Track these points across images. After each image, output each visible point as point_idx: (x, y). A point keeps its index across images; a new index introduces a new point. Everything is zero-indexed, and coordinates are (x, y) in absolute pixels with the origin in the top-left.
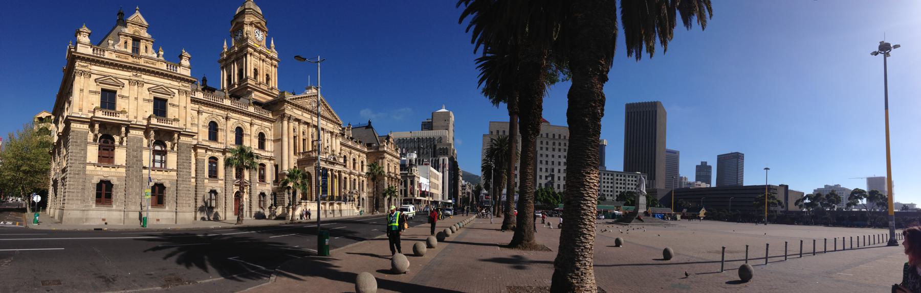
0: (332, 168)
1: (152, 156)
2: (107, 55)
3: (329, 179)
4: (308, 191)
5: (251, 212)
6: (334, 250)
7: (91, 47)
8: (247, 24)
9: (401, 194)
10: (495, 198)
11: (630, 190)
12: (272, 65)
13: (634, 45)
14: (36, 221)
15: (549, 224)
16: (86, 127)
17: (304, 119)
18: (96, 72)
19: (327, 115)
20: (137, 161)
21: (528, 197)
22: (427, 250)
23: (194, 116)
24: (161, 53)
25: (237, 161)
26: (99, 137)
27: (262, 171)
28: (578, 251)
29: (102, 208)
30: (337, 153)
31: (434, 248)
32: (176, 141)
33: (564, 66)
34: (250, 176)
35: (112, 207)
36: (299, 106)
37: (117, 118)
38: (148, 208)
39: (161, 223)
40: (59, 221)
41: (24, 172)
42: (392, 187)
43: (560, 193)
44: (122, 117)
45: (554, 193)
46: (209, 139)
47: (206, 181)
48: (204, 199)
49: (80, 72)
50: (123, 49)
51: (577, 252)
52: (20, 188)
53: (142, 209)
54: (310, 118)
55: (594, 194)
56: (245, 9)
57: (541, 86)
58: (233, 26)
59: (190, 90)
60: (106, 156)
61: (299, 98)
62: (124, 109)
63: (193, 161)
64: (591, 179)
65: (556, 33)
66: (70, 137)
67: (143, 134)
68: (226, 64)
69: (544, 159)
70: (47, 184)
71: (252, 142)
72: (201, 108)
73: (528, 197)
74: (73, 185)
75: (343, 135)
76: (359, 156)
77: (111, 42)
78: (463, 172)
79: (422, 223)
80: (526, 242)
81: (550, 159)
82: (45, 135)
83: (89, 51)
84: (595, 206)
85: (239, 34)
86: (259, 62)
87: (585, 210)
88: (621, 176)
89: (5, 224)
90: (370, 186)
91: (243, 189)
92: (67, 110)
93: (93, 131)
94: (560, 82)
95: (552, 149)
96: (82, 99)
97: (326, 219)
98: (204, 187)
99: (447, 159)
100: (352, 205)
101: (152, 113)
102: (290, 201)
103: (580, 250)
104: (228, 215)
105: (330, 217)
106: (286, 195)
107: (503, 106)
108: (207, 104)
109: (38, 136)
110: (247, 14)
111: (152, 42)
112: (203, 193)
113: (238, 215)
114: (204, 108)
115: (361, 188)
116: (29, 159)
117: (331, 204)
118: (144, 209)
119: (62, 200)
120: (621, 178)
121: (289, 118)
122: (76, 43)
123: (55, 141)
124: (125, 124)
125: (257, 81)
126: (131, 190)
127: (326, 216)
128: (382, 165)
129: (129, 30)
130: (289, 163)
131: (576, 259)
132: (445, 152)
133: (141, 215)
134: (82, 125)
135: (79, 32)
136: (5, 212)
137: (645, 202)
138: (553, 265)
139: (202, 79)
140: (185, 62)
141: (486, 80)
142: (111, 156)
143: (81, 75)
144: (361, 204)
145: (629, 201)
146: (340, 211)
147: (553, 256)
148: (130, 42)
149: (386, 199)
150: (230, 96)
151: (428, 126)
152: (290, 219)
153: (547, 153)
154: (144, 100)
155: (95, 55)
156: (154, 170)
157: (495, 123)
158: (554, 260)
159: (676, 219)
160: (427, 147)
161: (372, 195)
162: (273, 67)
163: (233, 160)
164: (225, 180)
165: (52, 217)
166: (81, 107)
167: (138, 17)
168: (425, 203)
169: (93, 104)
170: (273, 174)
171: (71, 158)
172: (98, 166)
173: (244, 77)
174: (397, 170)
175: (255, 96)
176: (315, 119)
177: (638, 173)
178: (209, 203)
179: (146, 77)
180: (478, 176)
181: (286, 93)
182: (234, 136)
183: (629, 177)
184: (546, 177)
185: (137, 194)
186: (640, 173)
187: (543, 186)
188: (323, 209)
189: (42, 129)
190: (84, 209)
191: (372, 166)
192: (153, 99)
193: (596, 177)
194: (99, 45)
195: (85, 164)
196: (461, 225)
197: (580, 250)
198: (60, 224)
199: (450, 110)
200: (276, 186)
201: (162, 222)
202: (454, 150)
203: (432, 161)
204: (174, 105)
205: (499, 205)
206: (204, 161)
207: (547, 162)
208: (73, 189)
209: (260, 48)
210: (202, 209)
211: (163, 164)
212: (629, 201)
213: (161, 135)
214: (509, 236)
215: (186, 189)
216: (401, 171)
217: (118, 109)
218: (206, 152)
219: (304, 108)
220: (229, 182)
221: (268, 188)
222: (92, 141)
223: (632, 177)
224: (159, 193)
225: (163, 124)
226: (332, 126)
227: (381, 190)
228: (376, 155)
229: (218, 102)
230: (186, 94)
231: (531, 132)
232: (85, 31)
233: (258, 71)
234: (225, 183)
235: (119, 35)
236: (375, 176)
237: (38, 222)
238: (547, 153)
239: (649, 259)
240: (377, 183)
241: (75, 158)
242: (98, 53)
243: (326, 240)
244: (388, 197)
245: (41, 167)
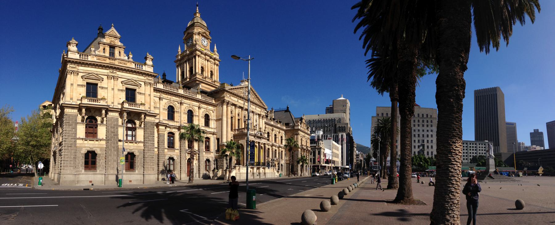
0: (259, 141)
1: (125, 132)
2: (90, 58)
3: (256, 150)
4: (241, 158)
5: (199, 174)
6: (260, 204)
7: (78, 54)
8: (196, 34)
9: (311, 162)
10: (381, 164)
11: (481, 154)
12: (215, 64)
13: (483, 44)
14: (40, 184)
15: (422, 183)
16: (76, 111)
17: (239, 104)
18: (82, 71)
19: (256, 101)
20: (114, 135)
21: (407, 163)
22: (331, 206)
23: (156, 101)
24: (131, 56)
25: (188, 135)
26: (85, 118)
27: (208, 143)
28: (447, 206)
29: (89, 172)
30: (263, 130)
31: (336, 204)
32: (143, 120)
33: (430, 62)
34: (199, 146)
35: (97, 171)
36: (235, 95)
37: (98, 104)
38: (122, 172)
39: (132, 184)
40: (58, 183)
41: (33, 146)
42: (304, 157)
43: (429, 158)
44: (102, 103)
45: (425, 158)
46: (168, 119)
47: (166, 150)
48: (164, 165)
49: (70, 71)
50: (102, 54)
51: (447, 207)
52: (30, 158)
53: (118, 173)
54: (237, 101)
55: (459, 159)
56: (194, 23)
57: (414, 78)
58: (186, 35)
59: (153, 82)
60: (91, 133)
61: (235, 88)
62: (104, 96)
63: (156, 135)
64: (457, 147)
65: (424, 37)
66: (64, 119)
67: (118, 115)
68: (180, 63)
69: (417, 133)
70: (49, 155)
71: (200, 121)
72: (162, 95)
73: (407, 163)
74: (67, 155)
75: (267, 116)
76: (279, 133)
77: (93, 49)
78: (357, 144)
79: (327, 184)
80: (407, 198)
81: (421, 133)
82: (47, 118)
83: (77, 56)
84: (460, 169)
85: (190, 42)
86: (204, 61)
87: (452, 172)
88: (473, 144)
89: (18, 186)
90: (287, 155)
91: (193, 156)
92: (62, 100)
93: (81, 114)
94: (427, 75)
95: (422, 126)
96: (72, 91)
97: (254, 180)
98: (165, 155)
99: (345, 135)
100: (274, 169)
101: (125, 100)
102: (227, 166)
103: (449, 205)
104: (182, 176)
105: (257, 178)
106: (225, 161)
107: (387, 94)
108: (166, 92)
109: (43, 119)
110: (196, 26)
111: (124, 48)
112: (163, 159)
113: (190, 176)
114: (164, 96)
115: (280, 156)
116: (36, 136)
117: (258, 169)
118: (120, 172)
119: (59, 167)
120: (473, 146)
121: (228, 103)
122: (67, 51)
123: (54, 122)
124: (105, 108)
125: (203, 76)
126: (110, 158)
127: (254, 178)
128: (297, 139)
129: (106, 40)
130: (227, 137)
131: (446, 213)
132: (343, 129)
133: (117, 177)
134: (73, 110)
135: (70, 44)
136: (19, 176)
137: (494, 163)
138: (429, 217)
139: (162, 74)
140: (149, 62)
141: (374, 75)
142: (95, 132)
143: (72, 74)
144: (280, 169)
145: (480, 163)
146: (265, 173)
147: (428, 209)
148: (108, 49)
149: (299, 166)
150: (183, 87)
151: (330, 110)
152: (227, 179)
153: (419, 128)
154: (119, 90)
155: (81, 59)
156: (127, 142)
157: (381, 108)
158: (430, 213)
159: (519, 176)
160: (330, 126)
161: (288, 162)
162: (216, 66)
163: (185, 135)
164: (180, 150)
165: (53, 180)
166: (72, 96)
167: (113, 31)
168: (329, 169)
169: (80, 94)
170: (215, 145)
171: (65, 134)
172: (85, 140)
173: (194, 73)
174: (308, 143)
175: (202, 86)
176: (246, 104)
177: (486, 141)
178: (168, 167)
179: (119, 74)
180: (368, 147)
181: (225, 85)
182: (186, 116)
183: (480, 144)
184: (419, 147)
185: (114, 161)
186: (488, 141)
187: (417, 154)
188: (252, 172)
189: (45, 114)
190: (75, 173)
191: (289, 140)
192: (125, 89)
193: (460, 145)
194: (84, 51)
195: (76, 139)
196: (356, 185)
197: (449, 205)
198: (58, 185)
199: (347, 98)
200: (218, 155)
201: (134, 183)
202: (350, 128)
203: (333, 136)
204: (140, 93)
205: (384, 169)
206: (164, 135)
207: (419, 135)
208: (67, 158)
209: (205, 52)
210: (163, 172)
211: (134, 138)
212: (480, 163)
213: (132, 116)
214: (393, 194)
215: (151, 156)
216: (310, 144)
217: (99, 97)
218: (166, 128)
219: (239, 96)
220: (183, 151)
221: (212, 156)
222: (80, 121)
223: (482, 145)
224: (131, 158)
225: (133, 108)
226: (259, 110)
227: (295, 159)
228: (292, 132)
229: (174, 91)
230: (150, 85)
231: (408, 113)
232: (73, 42)
233: (204, 68)
234: (180, 152)
235: (99, 44)
236: (291, 148)
237: (42, 184)
238: (419, 128)
239: (504, 209)
240: (293, 153)
241: (68, 135)
242: (83, 58)
243: (254, 197)
244: (301, 164)
245: (45, 142)
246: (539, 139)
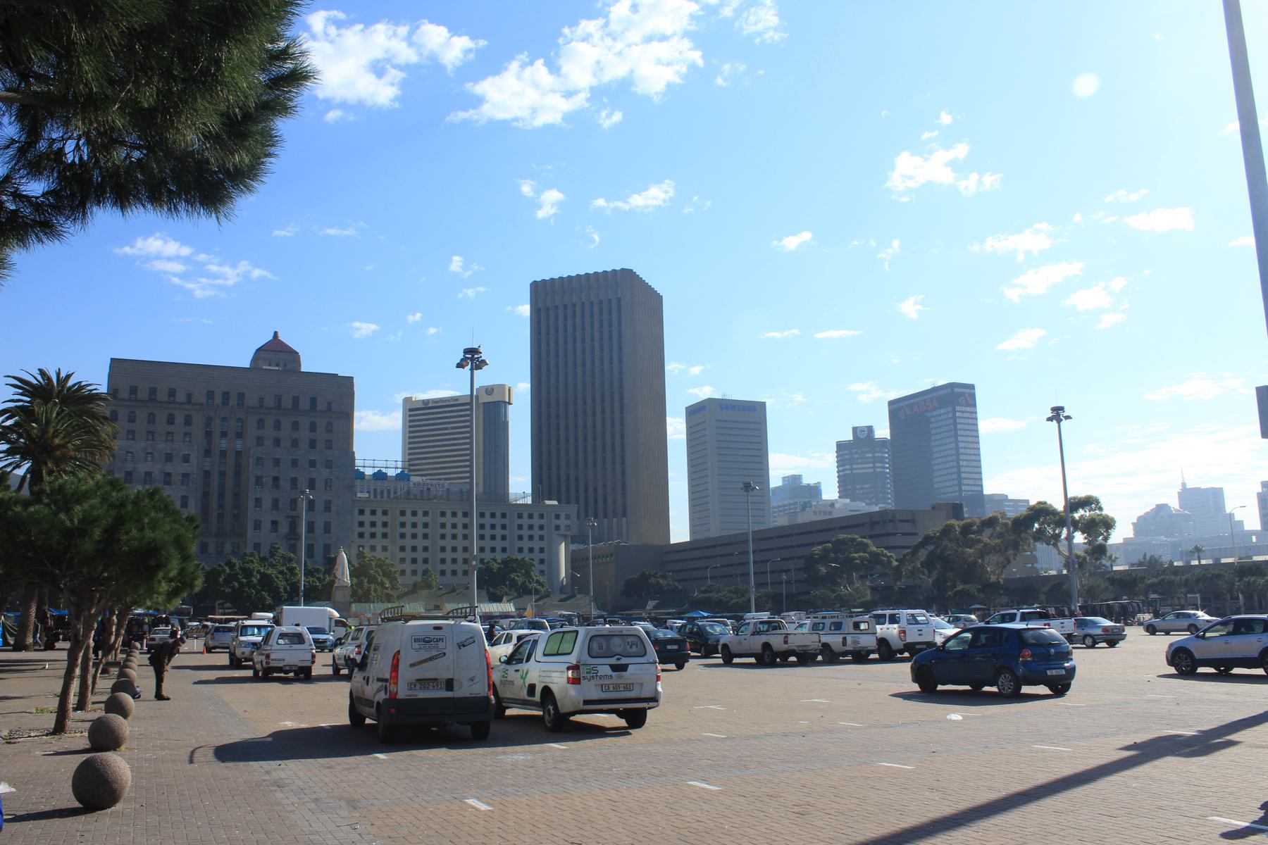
127: (7, 821)
246: (874, 468)
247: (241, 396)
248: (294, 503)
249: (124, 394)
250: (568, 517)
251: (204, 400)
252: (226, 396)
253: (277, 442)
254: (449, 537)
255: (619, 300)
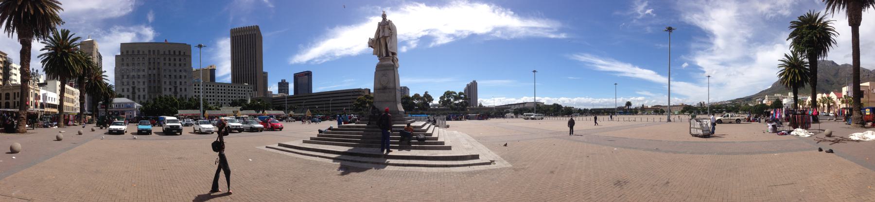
218: (472, 89)
247: (158, 51)
248: (175, 82)
249: (125, 53)
250: (251, 88)
251: (148, 53)
252: (154, 51)
253: (170, 64)
254: (220, 93)
255: (255, 34)
